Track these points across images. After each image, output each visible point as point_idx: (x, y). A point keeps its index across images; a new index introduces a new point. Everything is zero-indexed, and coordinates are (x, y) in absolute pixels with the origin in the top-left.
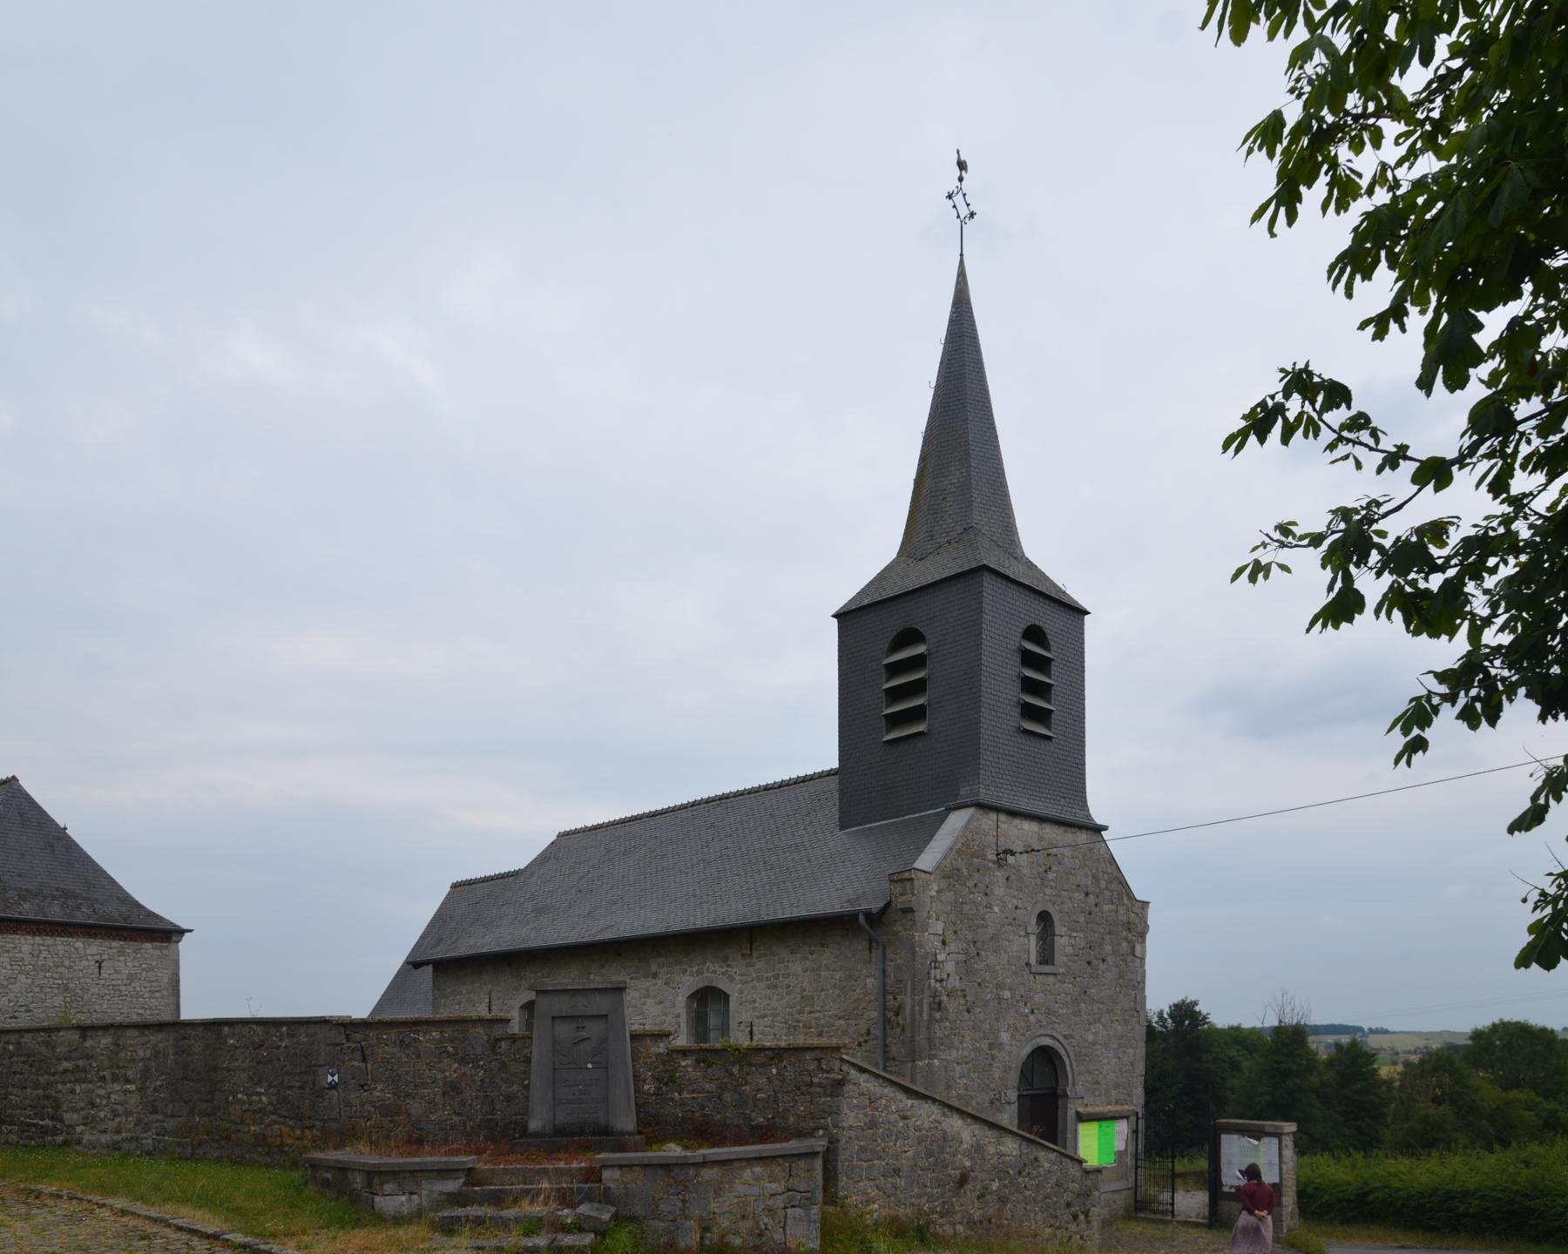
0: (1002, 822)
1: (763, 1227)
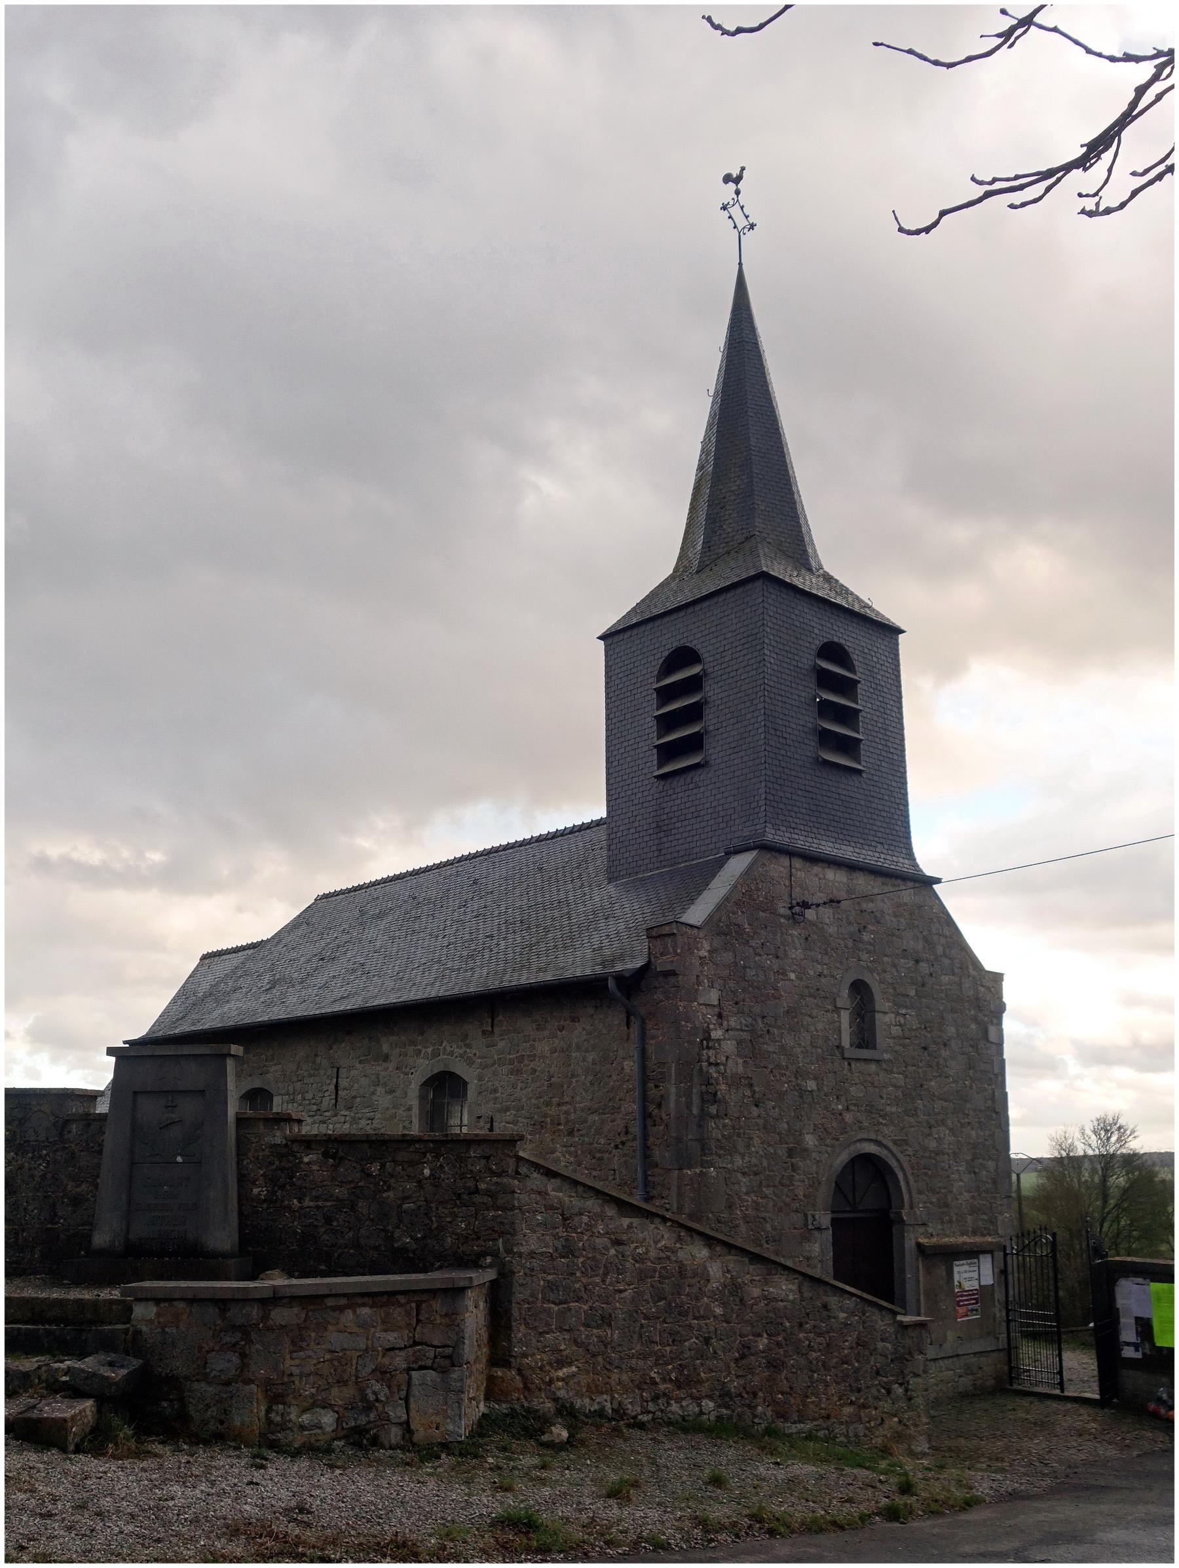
0: (797, 870)
1: (372, 1397)
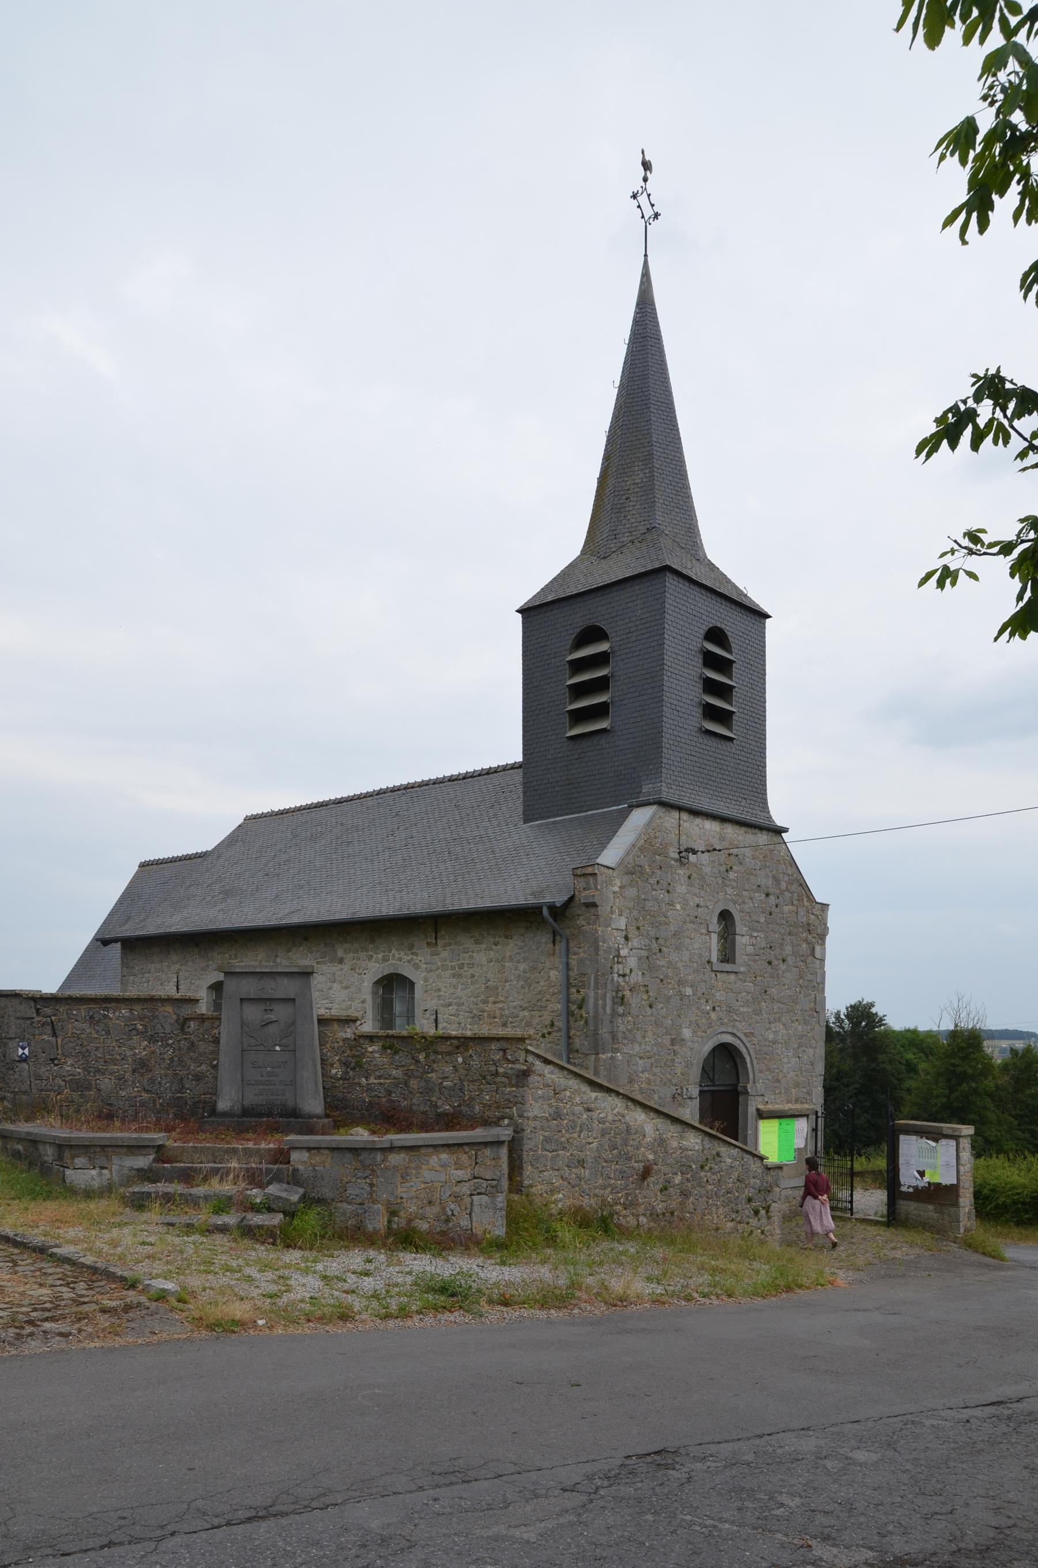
1: (450, 1213)
